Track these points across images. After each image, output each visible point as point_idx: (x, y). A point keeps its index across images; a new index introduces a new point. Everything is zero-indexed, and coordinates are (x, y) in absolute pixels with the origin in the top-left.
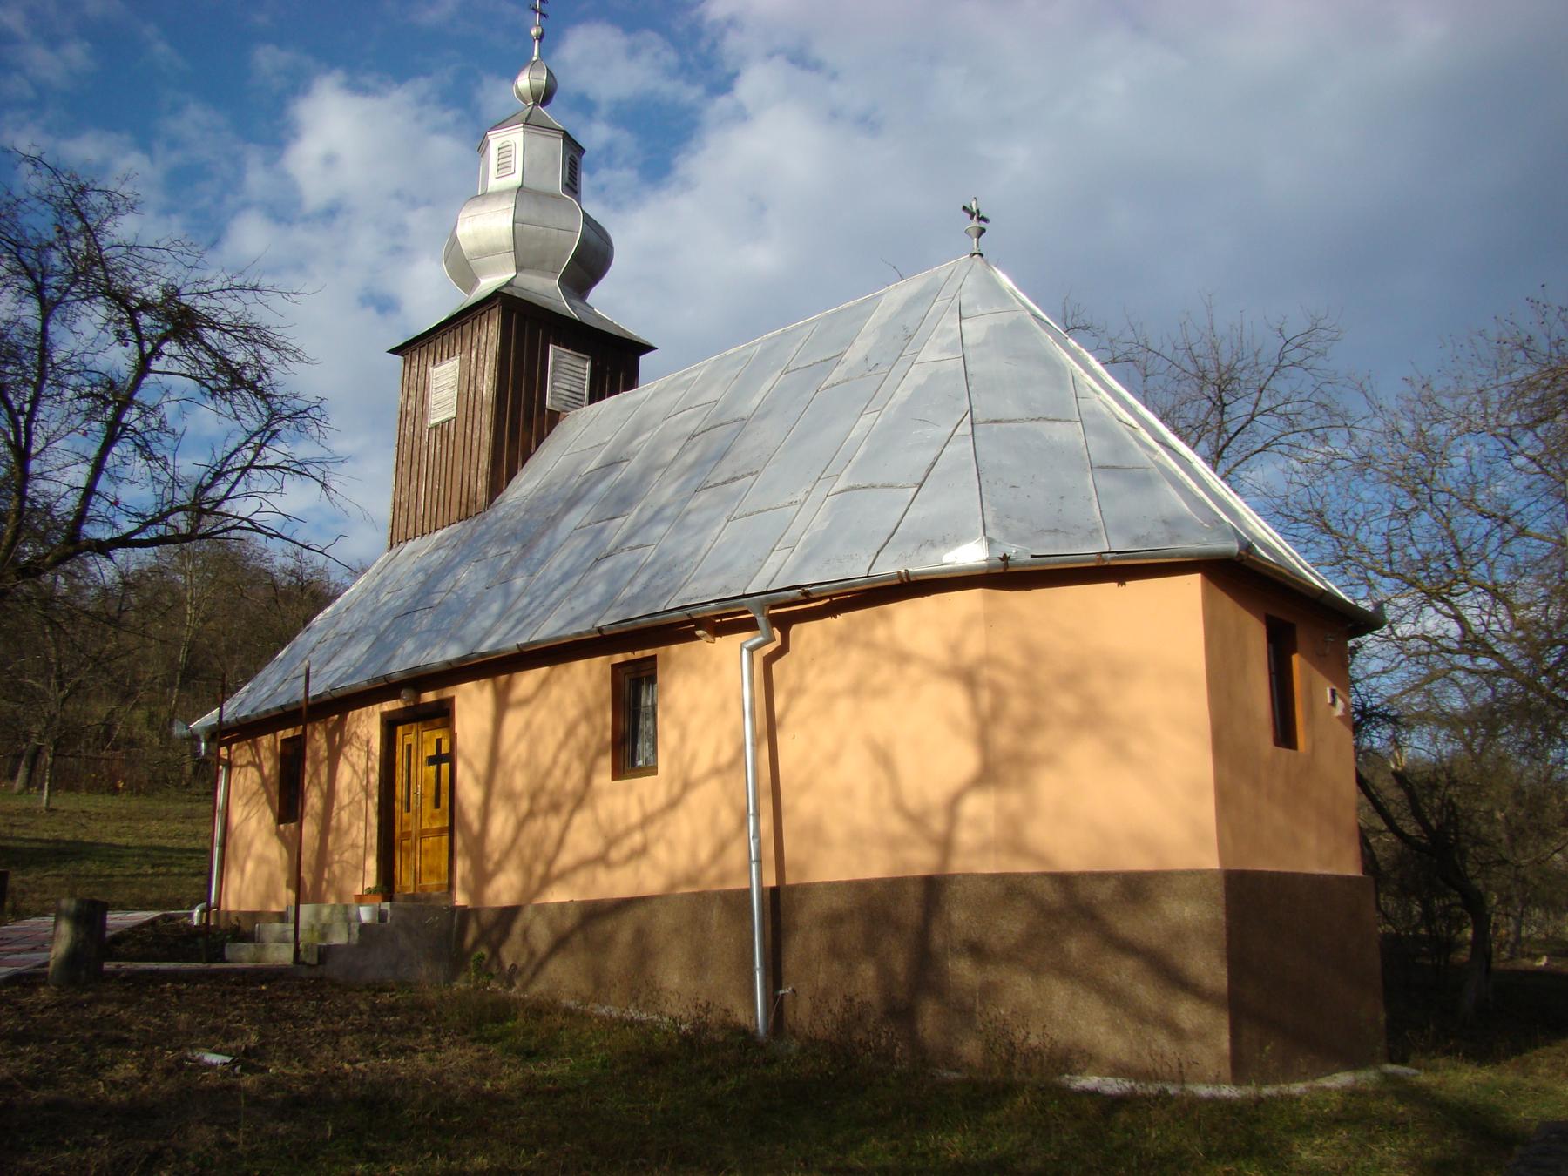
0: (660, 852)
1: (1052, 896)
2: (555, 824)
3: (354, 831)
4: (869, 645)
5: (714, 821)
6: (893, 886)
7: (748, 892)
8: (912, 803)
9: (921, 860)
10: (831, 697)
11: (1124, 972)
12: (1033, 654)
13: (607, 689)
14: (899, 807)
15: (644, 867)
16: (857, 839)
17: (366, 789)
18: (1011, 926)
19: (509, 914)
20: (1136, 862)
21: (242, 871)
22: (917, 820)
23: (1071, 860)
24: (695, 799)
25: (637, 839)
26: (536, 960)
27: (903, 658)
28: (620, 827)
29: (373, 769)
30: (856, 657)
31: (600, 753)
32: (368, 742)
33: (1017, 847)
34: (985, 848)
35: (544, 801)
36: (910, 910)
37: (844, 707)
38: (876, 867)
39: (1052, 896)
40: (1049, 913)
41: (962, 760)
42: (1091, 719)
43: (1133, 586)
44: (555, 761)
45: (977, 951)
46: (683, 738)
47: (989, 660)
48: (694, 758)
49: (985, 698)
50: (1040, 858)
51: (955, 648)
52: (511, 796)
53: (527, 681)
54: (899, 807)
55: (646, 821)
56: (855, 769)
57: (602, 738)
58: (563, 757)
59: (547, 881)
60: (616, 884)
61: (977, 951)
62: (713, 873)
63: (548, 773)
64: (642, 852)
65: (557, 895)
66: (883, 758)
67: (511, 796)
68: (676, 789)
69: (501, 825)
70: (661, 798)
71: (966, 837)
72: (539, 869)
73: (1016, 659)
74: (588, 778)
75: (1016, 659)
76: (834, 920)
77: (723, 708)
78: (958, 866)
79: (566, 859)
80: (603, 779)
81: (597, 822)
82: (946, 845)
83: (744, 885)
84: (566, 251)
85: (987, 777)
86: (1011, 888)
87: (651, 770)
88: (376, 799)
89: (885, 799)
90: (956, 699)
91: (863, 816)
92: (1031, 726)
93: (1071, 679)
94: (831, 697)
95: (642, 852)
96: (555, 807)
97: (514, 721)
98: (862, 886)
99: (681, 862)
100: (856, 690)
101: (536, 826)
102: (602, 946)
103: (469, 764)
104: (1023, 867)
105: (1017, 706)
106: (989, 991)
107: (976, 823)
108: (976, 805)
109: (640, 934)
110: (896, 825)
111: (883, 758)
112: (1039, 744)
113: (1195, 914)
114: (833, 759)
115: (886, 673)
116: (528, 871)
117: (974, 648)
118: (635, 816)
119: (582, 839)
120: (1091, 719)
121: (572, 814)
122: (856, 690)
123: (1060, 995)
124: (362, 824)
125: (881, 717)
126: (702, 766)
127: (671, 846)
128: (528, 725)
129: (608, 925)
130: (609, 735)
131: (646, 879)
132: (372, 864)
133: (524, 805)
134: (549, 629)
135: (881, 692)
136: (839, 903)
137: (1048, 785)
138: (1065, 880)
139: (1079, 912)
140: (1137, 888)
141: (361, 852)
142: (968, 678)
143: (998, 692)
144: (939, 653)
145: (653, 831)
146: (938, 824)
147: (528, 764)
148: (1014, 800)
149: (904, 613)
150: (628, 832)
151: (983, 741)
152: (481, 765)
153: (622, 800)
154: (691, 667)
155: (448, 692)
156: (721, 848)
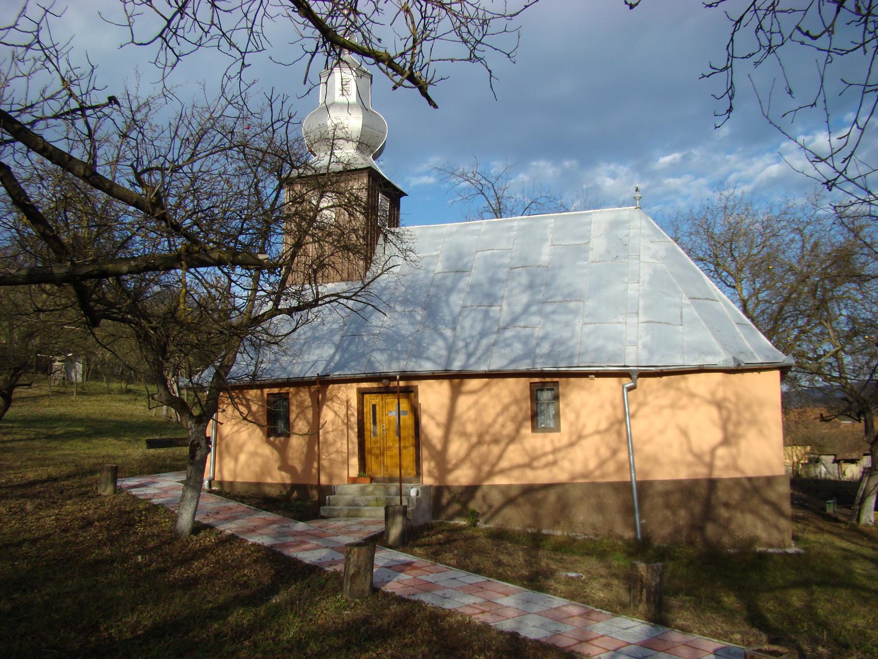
0: (566, 464)
1: (747, 484)
2: (496, 450)
3: (339, 445)
4: (678, 389)
5: (597, 451)
6: (695, 482)
7: (631, 482)
8: (696, 449)
9: (701, 472)
10: (662, 408)
11: (765, 510)
12: (738, 397)
13: (528, 392)
14: (691, 451)
15: (555, 470)
16: (674, 463)
17: (348, 425)
18: (736, 496)
19: (471, 490)
20: (767, 473)
21: (236, 459)
22: (698, 457)
23: (751, 473)
24: (585, 443)
25: (550, 458)
26: (493, 510)
27: (692, 395)
28: (539, 452)
29: (353, 415)
30: (672, 393)
31: (525, 419)
32: (347, 402)
33: (736, 468)
34: (727, 467)
35: (487, 438)
36: (703, 491)
37: (667, 412)
38: (683, 475)
39: (747, 484)
40: (745, 490)
41: (716, 435)
42: (753, 422)
43: (762, 373)
44: (495, 421)
45: (727, 505)
46: (578, 417)
47: (725, 399)
48: (584, 426)
49: (725, 413)
50: (742, 471)
51: (713, 394)
52: (464, 434)
53: (474, 384)
54: (691, 451)
55: (555, 451)
56: (672, 436)
57: (526, 413)
58: (501, 420)
59: (491, 474)
60: (542, 476)
61: (727, 505)
62: (597, 473)
63: (491, 425)
64: (554, 463)
65: (500, 481)
66: (684, 433)
67: (464, 434)
68: (574, 438)
69: (457, 448)
70: (565, 441)
71: (718, 463)
72: (486, 468)
73: (733, 399)
74: (518, 430)
75: (733, 399)
76: (666, 494)
77: (602, 406)
78: (717, 474)
79: (504, 464)
80: (527, 430)
81: (524, 450)
82: (711, 466)
83: (629, 480)
84: (738, 316)
85: (726, 441)
86: (737, 482)
87: (557, 429)
88: (356, 430)
89: (685, 448)
90: (714, 412)
91: (676, 454)
92: (738, 424)
93: (748, 407)
94: (662, 408)
95: (554, 463)
96: (496, 441)
97: (464, 402)
98: (678, 483)
99: (579, 468)
100: (673, 406)
101: (484, 449)
102: (537, 504)
103: (432, 417)
104: (737, 475)
105: (734, 417)
106: (729, 520)
107: (722, 458)
108: (721, 452)
109: (559, 498)
110: (690, 458)
111: (684, 433)
112: (741, 430)
113: (784, 489)
114: (662, 432)
115: (685, 400)
116: (479, 468)
117: (720, 395)
118: (549, 448)
119: (514, 455)
120: (753, 422)
121: (508, 445)
122: (673, 406)
123: (749, 519)
124: (345, 442)
125: (682, 417)
126: (589, 429)
127: (572, 461)
128: (476, 403)
129: (540, 495)
130: (530, 412)
131: (560, 475)
132: (355, 461)
133: (474, 439)
134: (496, 364)
135: (683, 408)
136: (670, 487)
137: (743, 444)
138: (750, 479)
139: (754, 489)
140: (770, 481)
141: (345, 455)
142: (719, 405)
143: (729, 412)
144: (708, 396)
145: (560, 455)
146: (707, 458)
147: (476, 420)
148: (734, 450)
149: (692, 377)
150: (545, 454)
151: (724, 428)
152: (442, 418)
153: (536, 441)
154: (582, 388)
155: (415, 383)
156: (602, 463)
